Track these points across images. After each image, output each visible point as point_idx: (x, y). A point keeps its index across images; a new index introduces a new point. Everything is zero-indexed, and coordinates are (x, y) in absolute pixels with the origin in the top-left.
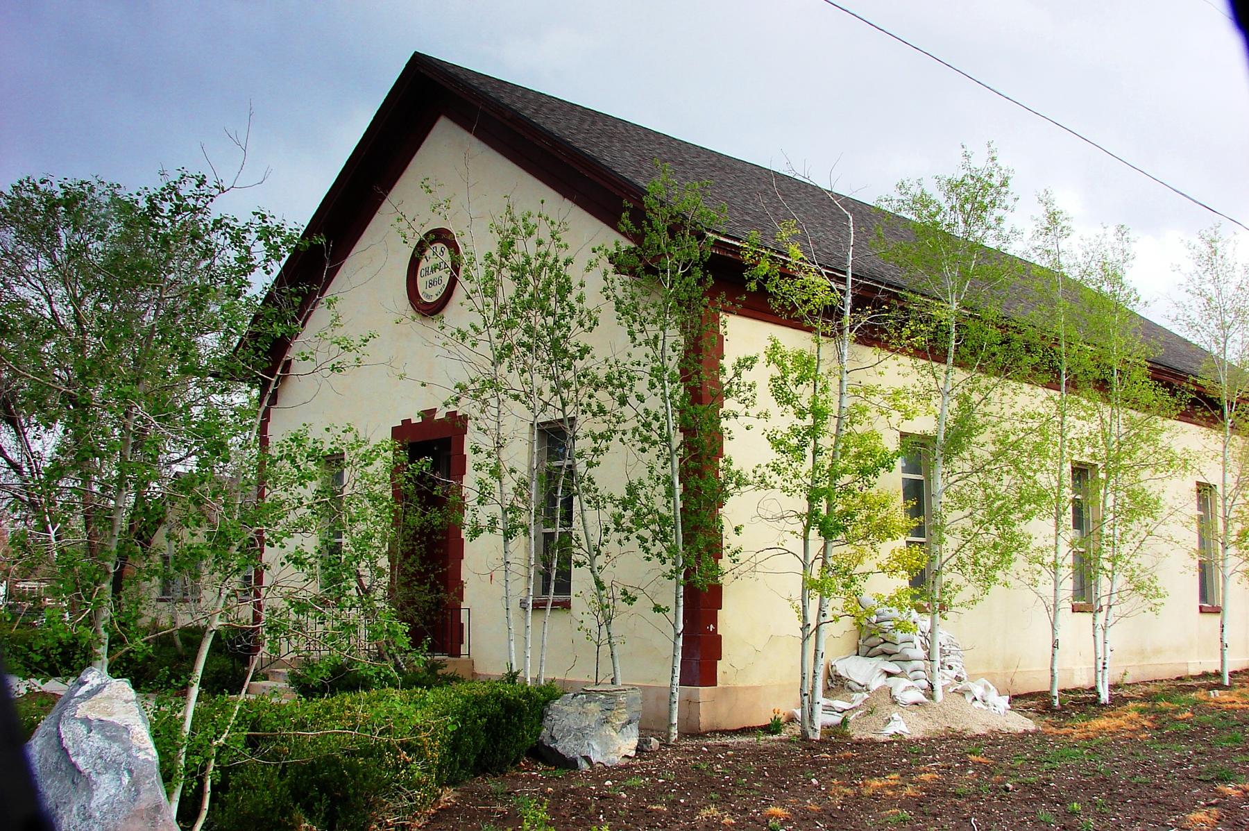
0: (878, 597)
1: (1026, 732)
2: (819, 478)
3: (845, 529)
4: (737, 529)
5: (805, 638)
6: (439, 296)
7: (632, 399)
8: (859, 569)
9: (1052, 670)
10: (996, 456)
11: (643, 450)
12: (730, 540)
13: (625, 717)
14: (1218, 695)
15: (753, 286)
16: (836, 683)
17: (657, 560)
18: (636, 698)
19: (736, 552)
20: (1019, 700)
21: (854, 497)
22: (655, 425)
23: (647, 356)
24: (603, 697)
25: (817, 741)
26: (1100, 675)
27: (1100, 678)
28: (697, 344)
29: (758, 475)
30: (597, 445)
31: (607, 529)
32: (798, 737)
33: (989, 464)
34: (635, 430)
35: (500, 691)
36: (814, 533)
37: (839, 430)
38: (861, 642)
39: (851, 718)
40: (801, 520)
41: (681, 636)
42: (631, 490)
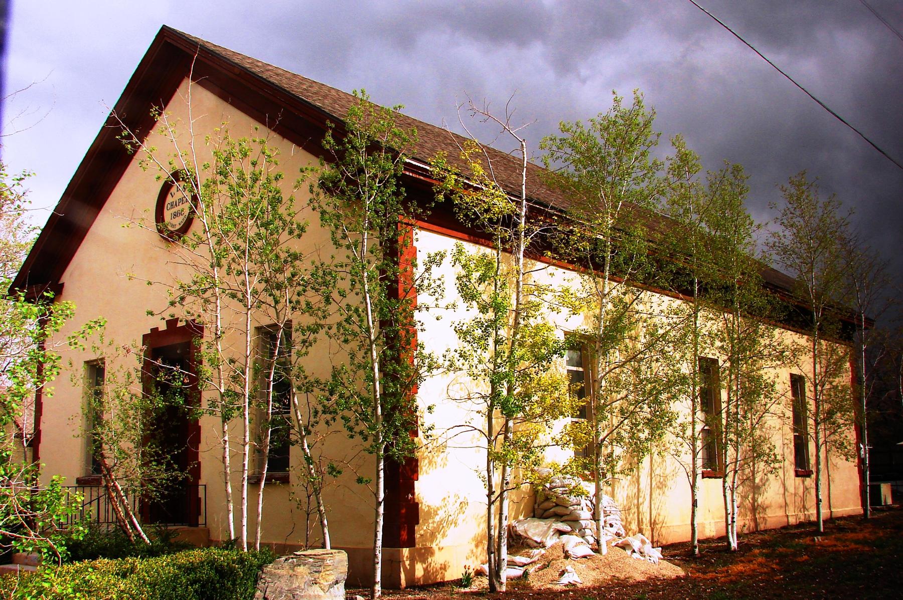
0: (554, 466)
1: (678, 578)
2: (501, 364)
3: (523, 409)
4: (429, 408)
5: (490, 504)
6: (181, 225)
7: (335, 295)
8: (536, 443)
9: (693, 525)
10: (650, 346)
11: (346, 341)
12: (425, 419)
13: (332, 578)
14: (820, 540)
15: (441, 197)
16: (518, 542)
17: (358, 438)
18: (342, 561)
19: (430, 429)
20: (672, 551)
21: (530, 381)
22: (355, 318)
23: (348, 257)
24: (311, 560)
25: (503, 592)
26: (730, 527)
27: (730, 530)
28: (393, 247)
29: (447, 359)
30: (305, 337)
31: (316, 412)
32: (486, 589)
33: (641, 352)
34: (339, 325)
35: (214, 558)
36: (496, 412)
37: (517, 323)
38: (536, 506)
39: (531, 570)
40: (486, 401)
41: (382, 504)
42: (336, 374)
